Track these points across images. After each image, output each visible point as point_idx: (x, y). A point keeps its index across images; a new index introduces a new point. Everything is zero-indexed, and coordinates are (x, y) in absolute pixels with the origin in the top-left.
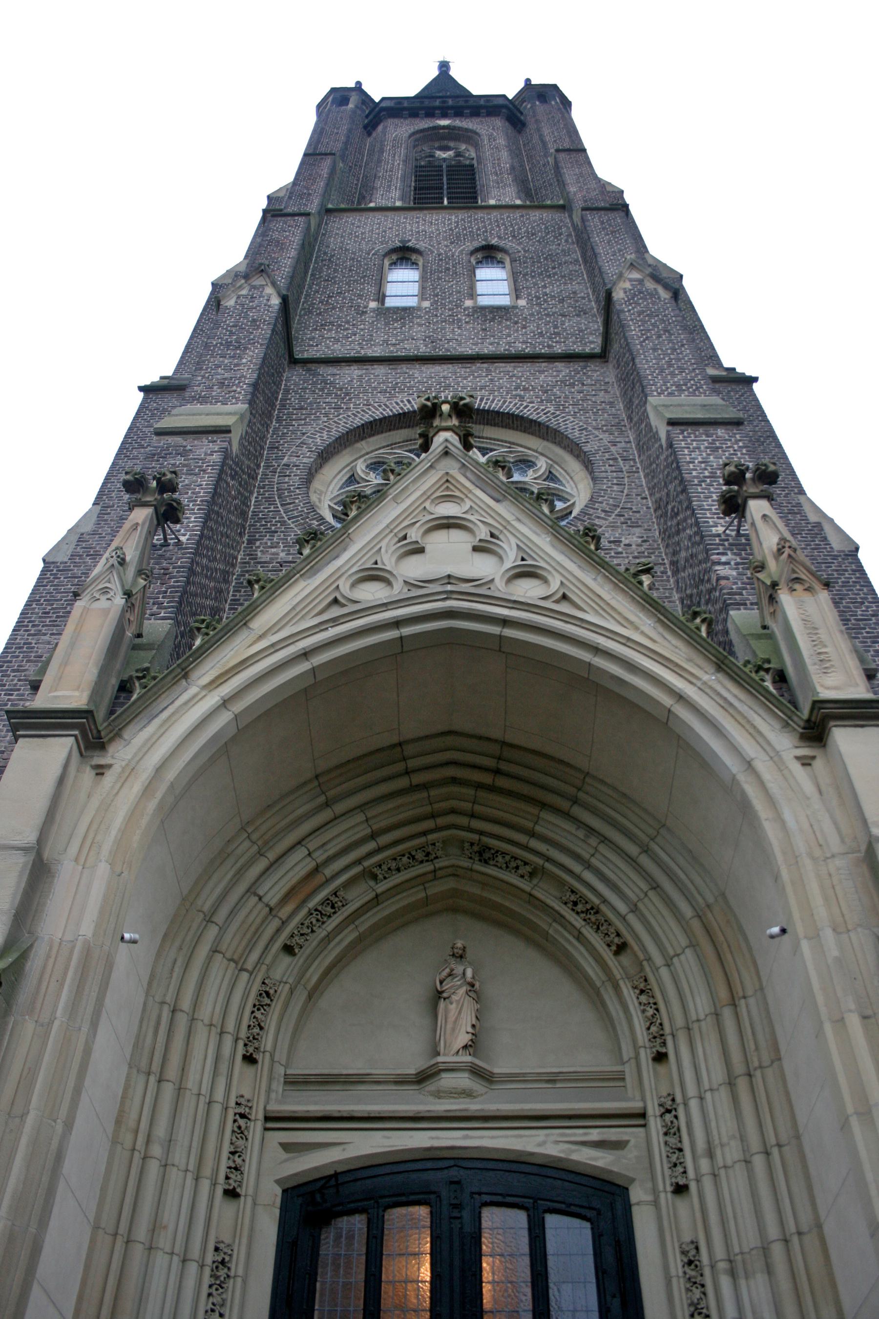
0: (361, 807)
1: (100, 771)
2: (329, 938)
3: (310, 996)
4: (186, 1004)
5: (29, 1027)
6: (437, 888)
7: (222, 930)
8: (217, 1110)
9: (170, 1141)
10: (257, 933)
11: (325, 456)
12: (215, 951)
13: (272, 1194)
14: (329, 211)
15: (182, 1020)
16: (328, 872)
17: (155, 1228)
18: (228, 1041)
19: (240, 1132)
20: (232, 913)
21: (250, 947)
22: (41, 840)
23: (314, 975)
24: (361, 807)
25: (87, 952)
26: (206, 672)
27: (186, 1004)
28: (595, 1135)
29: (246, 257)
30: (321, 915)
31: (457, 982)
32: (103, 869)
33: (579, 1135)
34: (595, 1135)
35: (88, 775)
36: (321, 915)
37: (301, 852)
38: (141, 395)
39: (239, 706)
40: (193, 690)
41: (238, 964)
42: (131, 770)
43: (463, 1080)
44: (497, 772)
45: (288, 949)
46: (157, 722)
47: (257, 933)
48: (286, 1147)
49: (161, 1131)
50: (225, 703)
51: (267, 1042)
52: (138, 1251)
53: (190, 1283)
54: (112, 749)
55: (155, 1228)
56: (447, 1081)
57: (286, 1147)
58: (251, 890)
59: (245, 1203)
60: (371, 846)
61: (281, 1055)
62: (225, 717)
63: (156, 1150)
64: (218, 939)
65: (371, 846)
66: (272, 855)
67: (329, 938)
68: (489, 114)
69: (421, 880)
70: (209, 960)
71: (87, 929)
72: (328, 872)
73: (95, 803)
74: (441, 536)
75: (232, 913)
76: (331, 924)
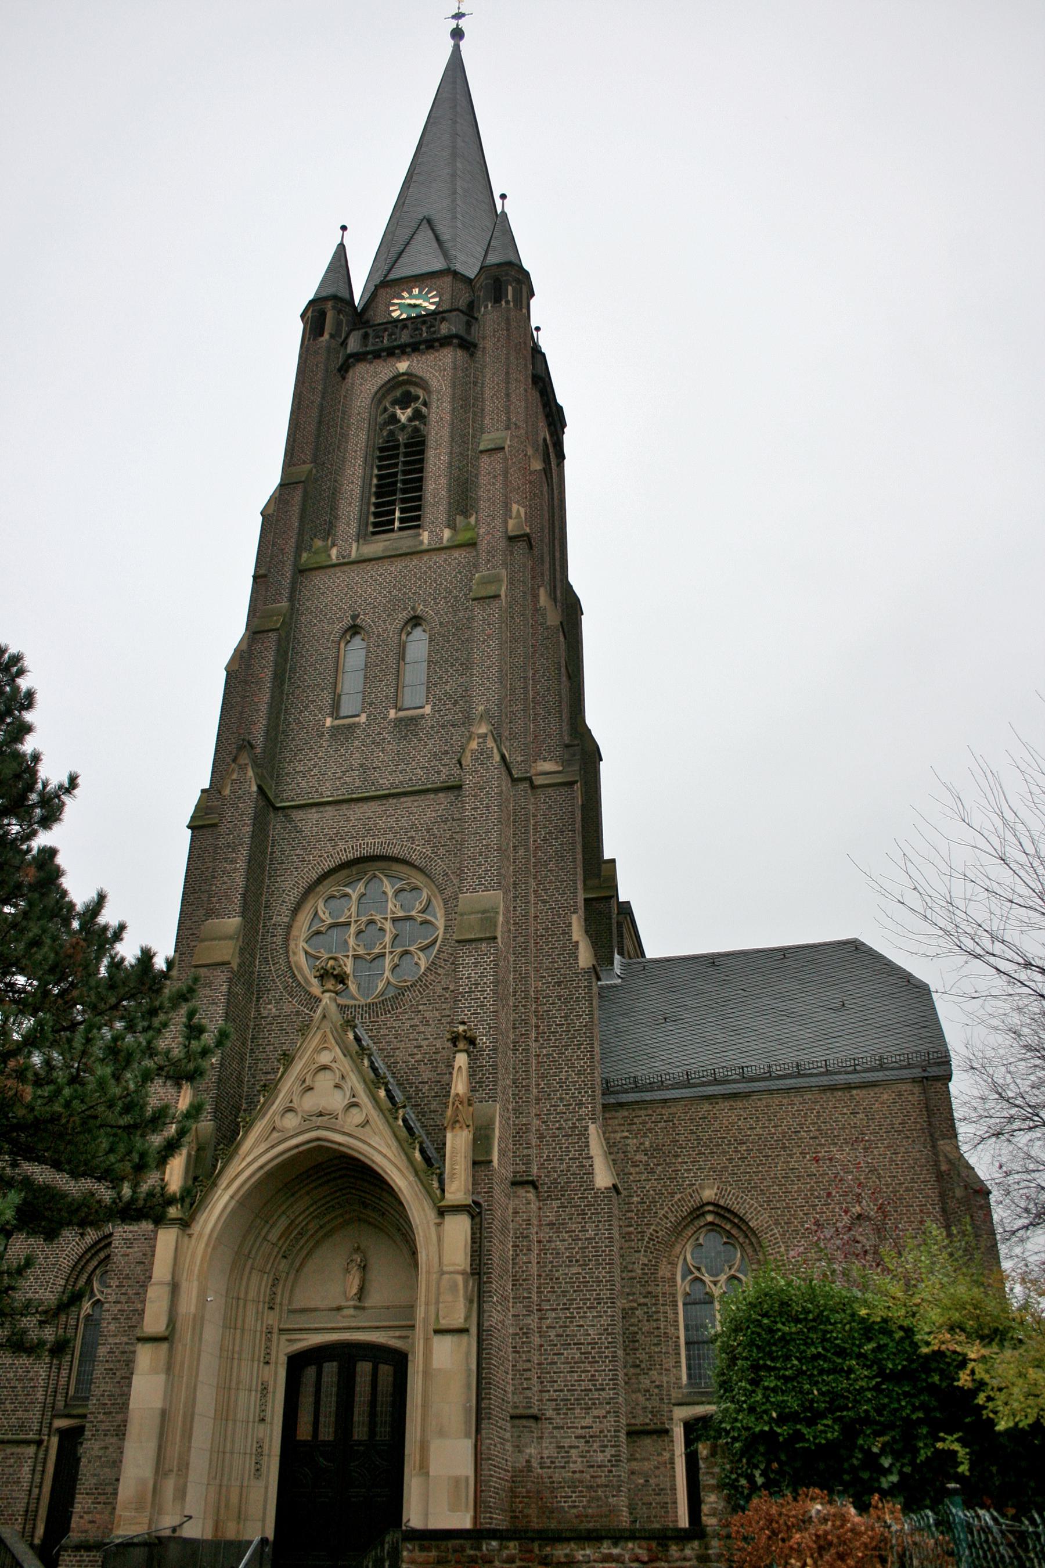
0: (308, 1193)
1: (190, 1236)
2: (302, 1248)
3: (297, 1271)
4: (242, 1296)
5: (180, 1347)
6: (347, 1216)
7: (254, 1259)
8: (258, 1334)
9: (241, 1350)
10: (270, 1254)
11: (296, 911)
12: (252, 1268)
13: (283, 1360)
14: (301, 572)
15: (241, 1302)
16: (297, 1222)
17: (238, 1383)
18: (261, 1304)
19: (269, 1340)
20: (258, 1250)
21: (267, 1262)
22: (173, 1278)
23: (297, 1264)
24: (308, 1193)
25: (195, 1316)
26: (223, 1182)
27: (242, 1296)
28: (397, 1334)
29: (247, 629)
30: (297, 1239)
31: (354, 1264)
32: (195, 1284)
33: (391, 1333)
34: (397, 1334)
35: (186, 1238)
36: (297, 1239)
37: (284, 1217)
38: (190, 831)
39: (237, 1198)
40: (219, 1192)
41: (262, 1271)
42: (200, 1235)
43: (351, 1312)
44: (230, 1389)
45: (284, 1257)
46: (207, 1210)
47: (270, 1254)
48: (289, 1341)
49: (237, 1349)
50: (232, 1197)
51: (278, 1300)
52: (233, 1392)
53: (253, 1398)
54: (193, 1225)
55: (238, 1383)
56: (346, 1312)
57: (289, 1341)
58: (265, 1238)
59: (272, 1366)
60: (315, 1207)
61: (285, 1301)
62: (233, 1203)
63: (236, 1356)
64: (252, 1265)
65: (315, 1207)
66: (271, 1222)
67: (302, 1248)
68: (442, 345)
69: (342, 1215)
70: (250, 1273)
71: (193, 1309)
72: (297, 1222)
73: (190, 1251)
74: (321, 1076)
75: (258, 1250)
76: (302, 1242)
